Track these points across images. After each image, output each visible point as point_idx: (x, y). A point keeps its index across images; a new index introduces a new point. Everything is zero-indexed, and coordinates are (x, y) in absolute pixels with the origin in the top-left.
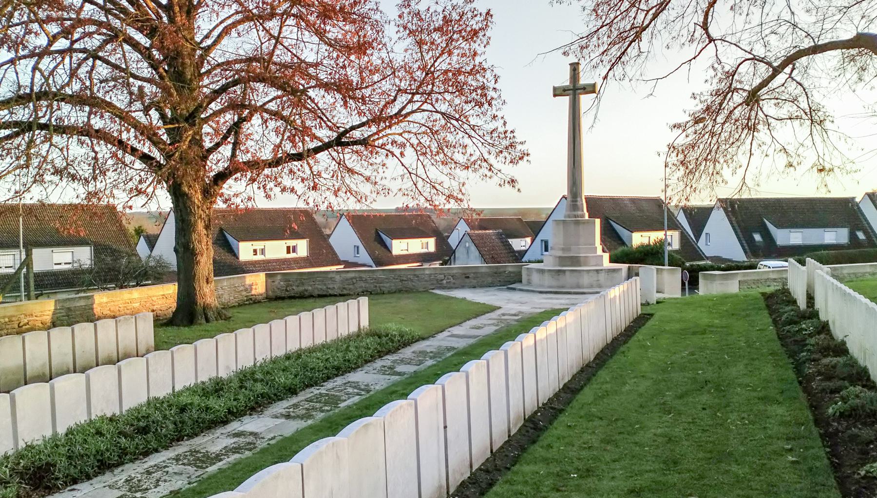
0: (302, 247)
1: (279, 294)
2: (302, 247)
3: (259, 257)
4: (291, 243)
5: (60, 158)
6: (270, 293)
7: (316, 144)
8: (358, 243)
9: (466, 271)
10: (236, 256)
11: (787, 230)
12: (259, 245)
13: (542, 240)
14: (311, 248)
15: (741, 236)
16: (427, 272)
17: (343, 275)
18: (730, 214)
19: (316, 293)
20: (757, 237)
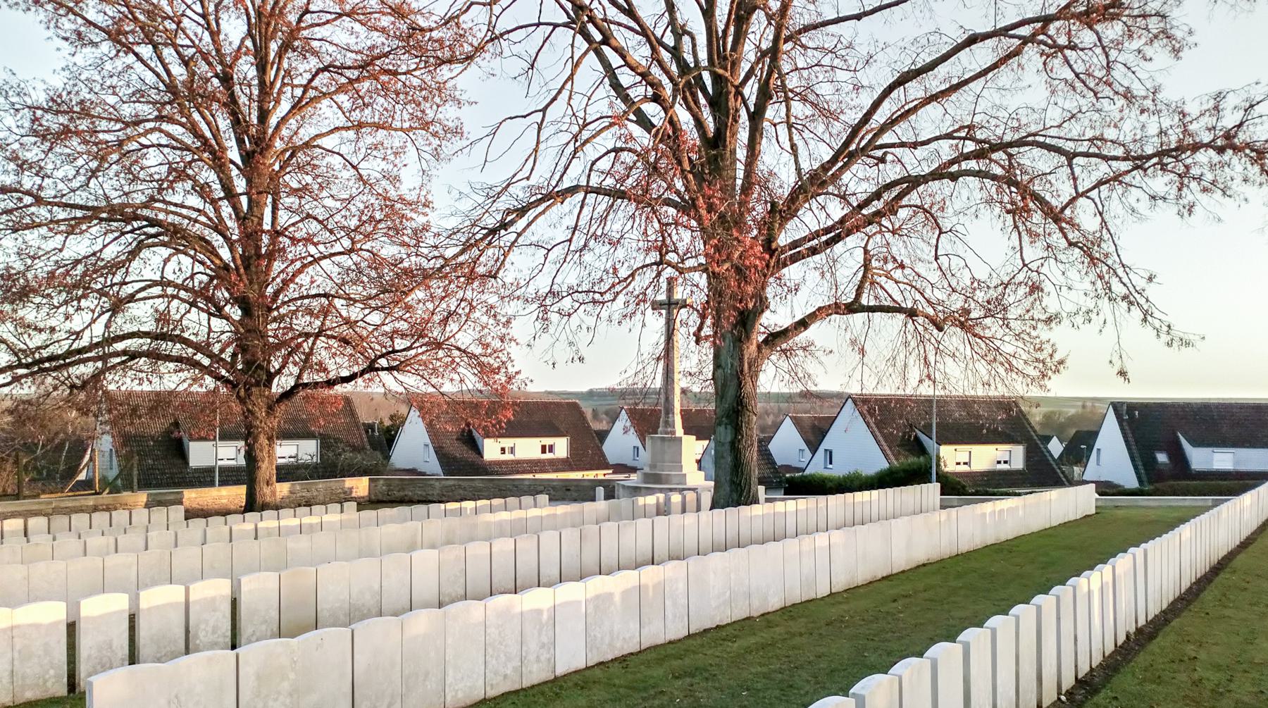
0: (561, 447)
1: (380, 497)
2: (561, 447)
3: (508, 457)
4: (547, 441)
5: (1051, 303)
6: (373, 497)
7: (337, 259)
8: (428, 441)
9: (567, 483)
10: (479, 453)
11: (1209, 450)
12: (507, 442)
13: (826, 450)
14: (572, 447)
15: (1136, 455)
16: (527, 483)
17: (443, 482)
18: (1125, 424)
19: (416, 498)
20: (1162, 458)
